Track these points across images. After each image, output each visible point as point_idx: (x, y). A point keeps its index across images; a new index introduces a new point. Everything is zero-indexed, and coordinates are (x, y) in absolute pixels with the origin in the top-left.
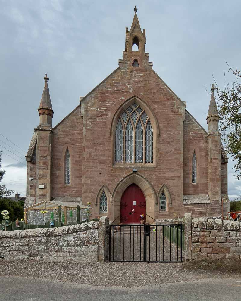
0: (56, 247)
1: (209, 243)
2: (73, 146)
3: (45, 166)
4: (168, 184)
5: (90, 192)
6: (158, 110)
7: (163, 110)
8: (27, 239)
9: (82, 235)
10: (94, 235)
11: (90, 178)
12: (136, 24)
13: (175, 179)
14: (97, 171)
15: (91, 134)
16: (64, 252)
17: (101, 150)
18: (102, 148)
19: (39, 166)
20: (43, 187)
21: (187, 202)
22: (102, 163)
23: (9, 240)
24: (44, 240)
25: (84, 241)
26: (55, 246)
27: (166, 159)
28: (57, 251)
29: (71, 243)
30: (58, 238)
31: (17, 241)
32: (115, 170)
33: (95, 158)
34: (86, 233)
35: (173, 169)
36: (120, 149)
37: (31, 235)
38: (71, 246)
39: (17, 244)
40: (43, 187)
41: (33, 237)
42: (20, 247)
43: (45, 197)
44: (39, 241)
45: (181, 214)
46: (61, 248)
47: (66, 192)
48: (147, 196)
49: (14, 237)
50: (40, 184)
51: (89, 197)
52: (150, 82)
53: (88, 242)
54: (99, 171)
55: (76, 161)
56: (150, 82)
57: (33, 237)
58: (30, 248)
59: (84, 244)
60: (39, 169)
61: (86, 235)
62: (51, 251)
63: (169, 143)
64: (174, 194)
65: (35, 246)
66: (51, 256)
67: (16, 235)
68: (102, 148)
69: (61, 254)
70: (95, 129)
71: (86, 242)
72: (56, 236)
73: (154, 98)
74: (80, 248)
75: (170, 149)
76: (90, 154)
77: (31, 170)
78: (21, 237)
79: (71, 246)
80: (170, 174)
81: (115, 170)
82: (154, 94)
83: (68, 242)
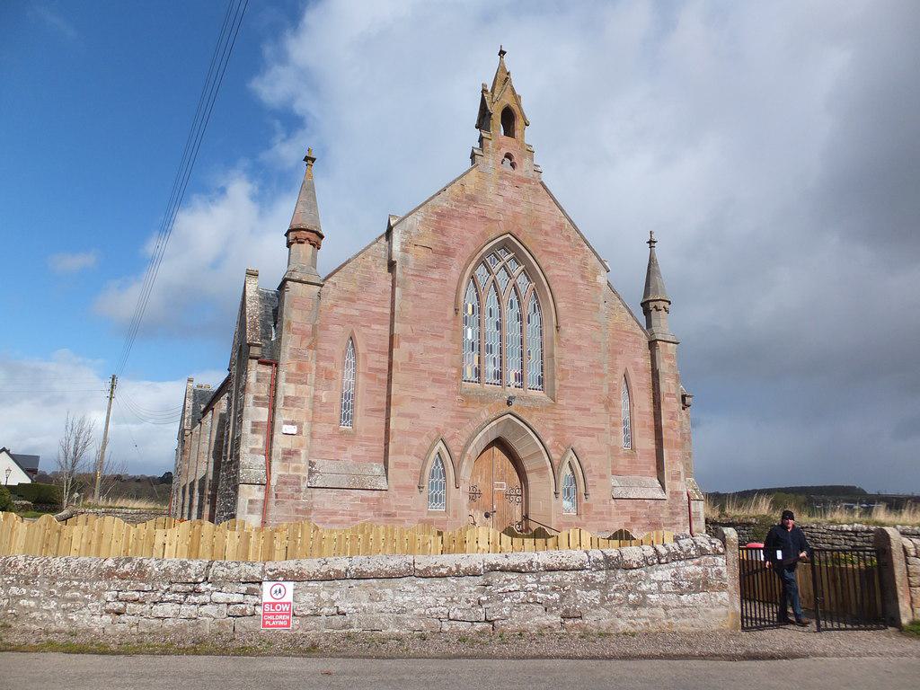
0: (631, 596)
1: (229, 604)
2: (364, 330)
3: (302, 376)
4: (580, 446)
5: (408, 453)
6: (556, 272)
7: (564, 273)
8: (558, 576)
9: (690, 568)
10: (716, 568)
11: (411, 416)
12: (503, 78)
13: (594, 436)
14: (426, 400)
15: (415, 306)
16: (652, 606)
17: (436, 349)
18: (438, 344)
19: (287, 374)
20: (293, 429)
21: (619, 492)
22: (438, 380)
23: (509, 576)
24: (600, 576)
25: (697, 582)
26: (629, 592)
27: (575, 385)
28: (635, 606)
29: (668, 587)
30: (634, 572)
31: (529, 578)
32: (467, 402)
33: (422, 367)
34: (699, 564)
35: (589, 410)
36: (473, 350)
37: (568, 567)
38: (668, 592)
39: (530, 587)
40: (293, 429)
41: (573, 569)
42: (539, 594)
43: (295, 458)
44: (587, 579)
45: (608, 523)
46: (645, 598)
47: (345, 449)
48: (532, 471)
49: (523, 570)
50: (287, 423)
51: (406, 465)
52: (538, 207)
53: (706, 583)
54: (431, 400)
55: (370, 369)
56: (538, 207)
57: (573, 569)
58: (565, 596)
59: (698, 588)
60: (287, 381)
61: (699, 569)
62: (620, 605)
63: (579, 347)
64: (594, 473)
65: (578, 591)
66: (619, 616)
67: (531, 564)
68: (438, 344)
69: (644, 612)
70: (424, 295)
71: (702, 584)
72: (632, 568)
73: (548, 243)
74: (690, 598)
75: (584, 364)
76: (411, 355)
77: (258, 380)
78: (541, 569)
79: (668, 592)
80: (586, 422)
81: (467, 402)
82: (546, 234)
83: (660, 583)
